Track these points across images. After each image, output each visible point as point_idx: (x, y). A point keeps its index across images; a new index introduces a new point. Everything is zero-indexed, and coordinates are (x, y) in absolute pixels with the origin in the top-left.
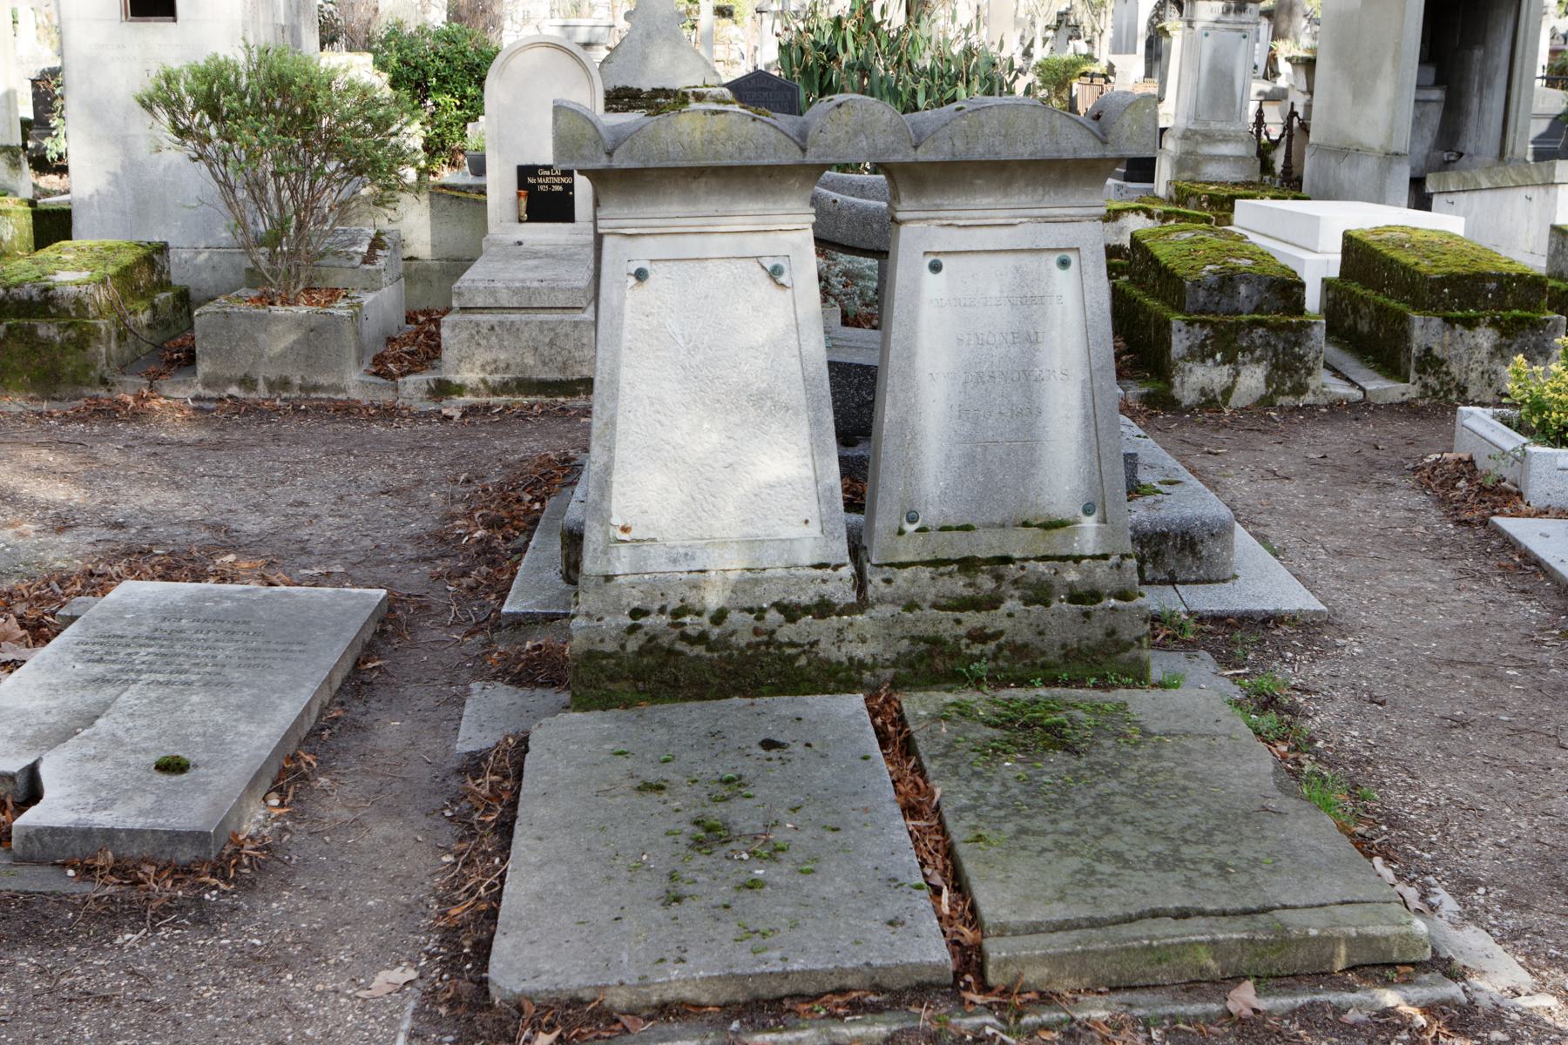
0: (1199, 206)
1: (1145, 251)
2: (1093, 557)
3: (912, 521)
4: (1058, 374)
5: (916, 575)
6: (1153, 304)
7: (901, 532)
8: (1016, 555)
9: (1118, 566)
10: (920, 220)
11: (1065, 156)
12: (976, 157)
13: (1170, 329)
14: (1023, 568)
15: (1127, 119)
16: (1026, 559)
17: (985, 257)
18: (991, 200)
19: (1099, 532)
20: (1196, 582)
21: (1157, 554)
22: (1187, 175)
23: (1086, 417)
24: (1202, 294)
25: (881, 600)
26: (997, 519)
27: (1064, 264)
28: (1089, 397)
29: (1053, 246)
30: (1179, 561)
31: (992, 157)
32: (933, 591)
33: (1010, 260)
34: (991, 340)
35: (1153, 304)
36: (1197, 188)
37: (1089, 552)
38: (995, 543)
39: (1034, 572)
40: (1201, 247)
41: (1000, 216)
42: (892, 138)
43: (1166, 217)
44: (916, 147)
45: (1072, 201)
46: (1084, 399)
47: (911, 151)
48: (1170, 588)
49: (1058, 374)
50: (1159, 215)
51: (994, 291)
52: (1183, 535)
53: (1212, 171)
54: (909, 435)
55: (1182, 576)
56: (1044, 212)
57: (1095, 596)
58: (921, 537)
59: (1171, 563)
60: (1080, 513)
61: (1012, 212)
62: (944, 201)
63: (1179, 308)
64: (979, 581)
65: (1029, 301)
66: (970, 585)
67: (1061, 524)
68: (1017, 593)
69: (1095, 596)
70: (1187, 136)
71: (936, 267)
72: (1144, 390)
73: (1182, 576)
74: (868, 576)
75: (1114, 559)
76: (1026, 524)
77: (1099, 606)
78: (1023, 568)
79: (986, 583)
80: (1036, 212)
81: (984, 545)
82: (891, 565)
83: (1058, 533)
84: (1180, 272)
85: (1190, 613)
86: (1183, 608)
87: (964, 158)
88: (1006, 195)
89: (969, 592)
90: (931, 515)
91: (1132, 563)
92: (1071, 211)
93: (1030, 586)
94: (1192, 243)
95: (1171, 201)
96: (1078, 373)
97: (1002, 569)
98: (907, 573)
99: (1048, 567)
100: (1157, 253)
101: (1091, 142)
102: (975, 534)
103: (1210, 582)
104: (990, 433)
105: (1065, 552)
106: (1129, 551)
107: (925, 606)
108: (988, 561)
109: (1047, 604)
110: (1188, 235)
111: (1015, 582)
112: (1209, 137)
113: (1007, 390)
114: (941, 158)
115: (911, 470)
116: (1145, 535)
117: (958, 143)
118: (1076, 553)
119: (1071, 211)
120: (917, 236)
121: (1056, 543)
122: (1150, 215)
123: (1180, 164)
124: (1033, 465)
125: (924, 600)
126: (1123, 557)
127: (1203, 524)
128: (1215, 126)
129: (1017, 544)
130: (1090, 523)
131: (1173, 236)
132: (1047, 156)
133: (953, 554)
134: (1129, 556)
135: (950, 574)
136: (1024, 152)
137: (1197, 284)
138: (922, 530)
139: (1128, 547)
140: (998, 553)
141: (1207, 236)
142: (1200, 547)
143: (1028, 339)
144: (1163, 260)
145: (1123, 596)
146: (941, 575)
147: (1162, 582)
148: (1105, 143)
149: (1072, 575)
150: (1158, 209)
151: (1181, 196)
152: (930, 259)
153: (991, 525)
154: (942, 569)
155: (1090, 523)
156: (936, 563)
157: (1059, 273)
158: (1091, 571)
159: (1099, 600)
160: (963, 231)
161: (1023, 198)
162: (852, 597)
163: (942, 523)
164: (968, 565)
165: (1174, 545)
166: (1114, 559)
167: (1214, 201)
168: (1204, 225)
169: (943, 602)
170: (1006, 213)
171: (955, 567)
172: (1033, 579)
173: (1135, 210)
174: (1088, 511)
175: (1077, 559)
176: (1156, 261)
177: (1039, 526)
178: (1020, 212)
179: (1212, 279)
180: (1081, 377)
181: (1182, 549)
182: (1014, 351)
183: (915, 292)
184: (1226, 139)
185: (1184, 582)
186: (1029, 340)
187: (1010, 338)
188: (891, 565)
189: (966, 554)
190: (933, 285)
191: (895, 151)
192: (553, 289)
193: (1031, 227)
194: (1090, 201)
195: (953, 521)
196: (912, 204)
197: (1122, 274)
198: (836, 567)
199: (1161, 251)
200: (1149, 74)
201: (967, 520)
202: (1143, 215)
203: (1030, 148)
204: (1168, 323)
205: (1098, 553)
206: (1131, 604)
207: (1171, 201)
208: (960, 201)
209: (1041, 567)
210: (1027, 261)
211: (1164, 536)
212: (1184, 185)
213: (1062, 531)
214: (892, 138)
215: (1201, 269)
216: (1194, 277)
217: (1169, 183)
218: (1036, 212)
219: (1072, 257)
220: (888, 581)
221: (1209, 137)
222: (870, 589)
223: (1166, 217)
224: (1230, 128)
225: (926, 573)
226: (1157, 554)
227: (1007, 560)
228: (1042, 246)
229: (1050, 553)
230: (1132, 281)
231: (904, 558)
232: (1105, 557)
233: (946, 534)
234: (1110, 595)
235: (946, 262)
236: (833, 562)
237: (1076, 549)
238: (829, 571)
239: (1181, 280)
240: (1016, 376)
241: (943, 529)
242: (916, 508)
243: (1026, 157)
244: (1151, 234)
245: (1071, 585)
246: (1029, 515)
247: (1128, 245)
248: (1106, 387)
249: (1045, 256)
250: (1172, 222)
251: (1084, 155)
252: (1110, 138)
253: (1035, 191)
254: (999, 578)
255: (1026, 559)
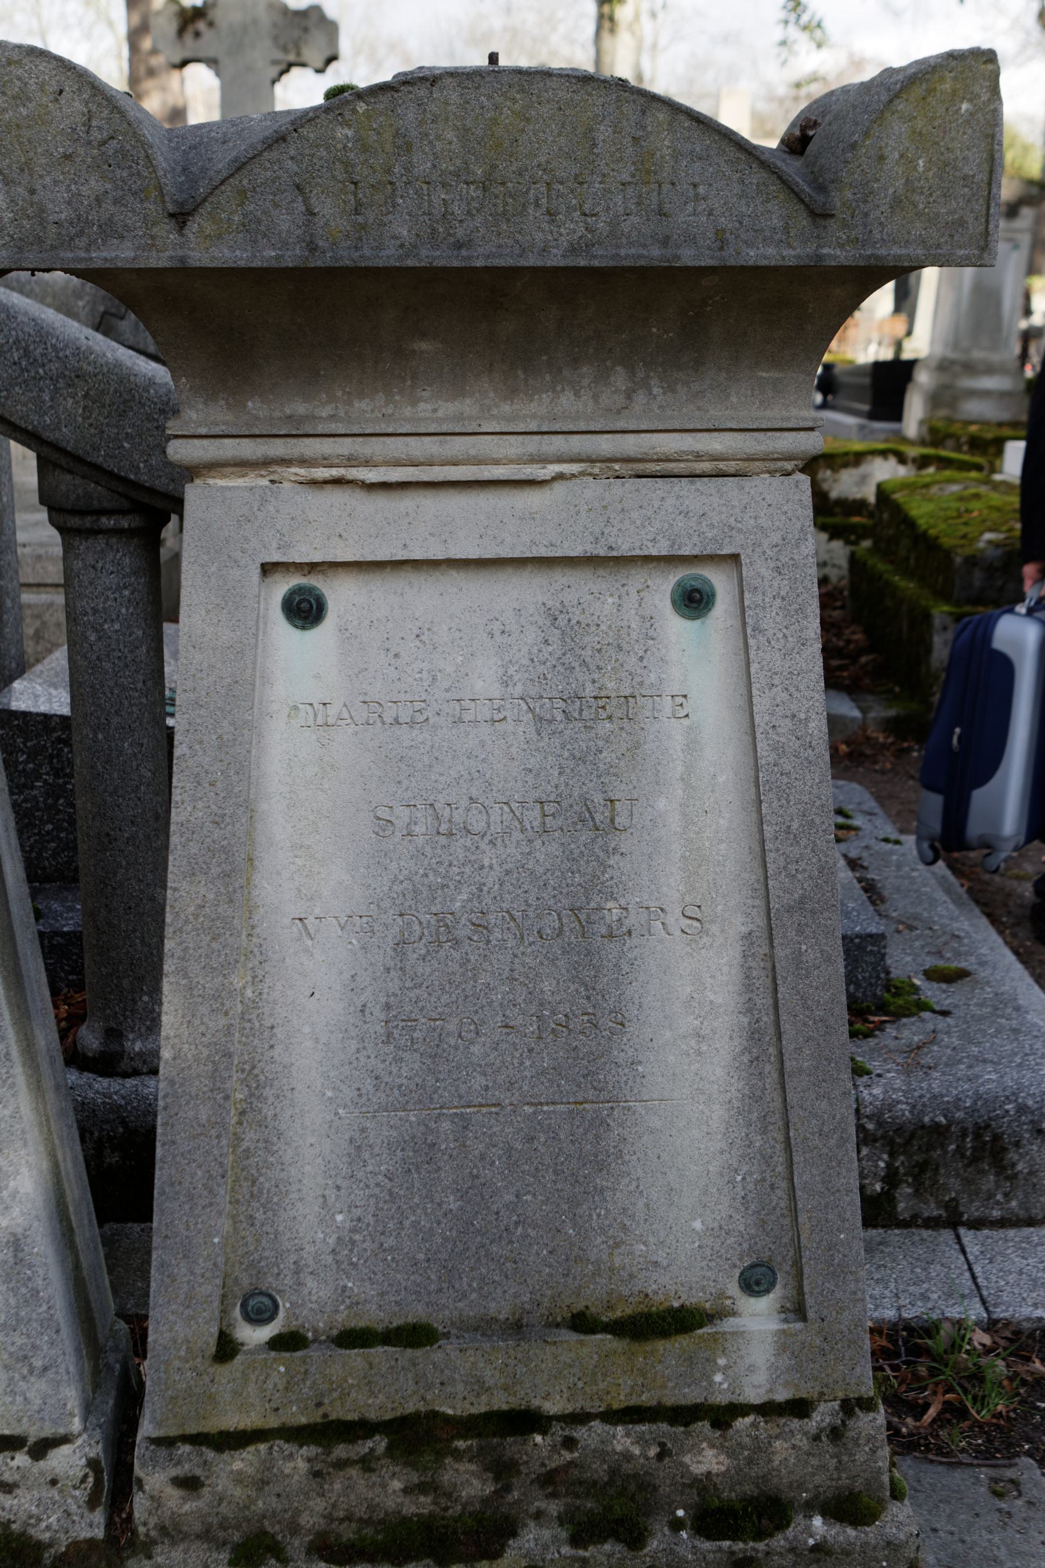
0: (958, 449)
1: (897, 509)
2: (768, 1410)
3: (258, 1317)
4: (674, 919)
5: (267, 1465)
6: (907, 586)
7: (226, 1348)
8: (551, 1407)
9: (836, 1434)
10: (243, 465)
11: (688, 257)
12: (388, 256)
13: (930, 625)
14: (570, 1443)
15: (896, 135)
16: (579, 1418)
17: (456, 577)
18: (467, 406)
19: (784, 1343)
20: (1002, 1223)
21: (922, 1167)
22: (943, 413)
23: (754, 1035)
24: (978, 577)
25: (171, 1532)
26: (501, 1308)
27: (694, 601)
28: (762, 982)
29: (662, 548)
30: (968, 1182)
31: (444, 258)
32: (319, 1505)
33: (528, 592)
34: (478, 824)
35: (907, 586)
36: (956, 428)
37: (753, 1396)
38: (491, 1376)
39: (602, 1454)
40: (975, 505)
41: (505, 457)
42: (95, 185)
43: (922, 462)
44: (180, 217)
45: (717, 414)
46: (748, 987)
47: (166, 232)
48: (947, 1235)
49: (674, 919)
50: (914, 460)
51: (484, 681)
52: (979, 1131)
53: (973, 408)
54: (247, 1086)
55: (973, 1210)
56: (630, 445)
57: (768, 1511)
58: (281, 1366)
59: (953, 1185)
60: (733, 1289)
61: (532, 445)
62: (324, 410)
63: (944, 595)
64: (446, 1477)
65: (588, 711)
66: (422, 1488)
67: (682, 1321)
68: (554, 1508)
69: (768, 1511)
70: (943, 366)
71: (304, 610)
72: (892, 713)
73: (973, 1210)
74: (138, 1471)
75: (823, 1415)
76: (582, 1323)
77: (779, 1541)
78: (570, 1443)
79: (468, 1482)
80: (605, 445)
81: (460, 1382)
82: (198, 1440)
83: (669, 1350)
84: (946, 542)
85: (991, 1326)
86: (975, 1312)
87: (347, 257)
88: (511, 393)
89: (423, 1505)
90: (314, 1299)
91: (873, 1423)
92: (716, 443)
93: (592, 1488)
94: (961, 499)
95: (922, 443)
96: (733, 919)
97: (511, 1447)
98: (242, 1461)
99: (641, 1440)
100: (914, 513)
101: (775, 213)
102: (436, 1355)
103: (1031, 1222)
104: (479, 1081)
105: (691, 1395)
106: (868, 1388)
107: (296, 1546)
108: (469, 1426)
109: (635, 1540)
110: (955, 488)
111: (549, 1480)
112: (970, 368)
113: (516, 971)
114: (267, 255)
115: (251, 1185)
116: (899, 1130)
117: (326, 208)
118: (721, 1399)
119: (716, 443)
120: (232, 522)
121: (664, 1372)
122: (902, 459)
123: (936, 399)
124: (601, 1167)
125: (294, 1529)
126: (849, 1407)
127: (1022, 1109)
128: (977, 355)
129: (556, 1377)
130: (758, 1317)
131: (934, 490)
132: (629, 254)
133: (376, 1406)
134: (867, 1405)
135: (366, 1464)
136: (548, 240)
137: (972, 561)
138: (288, 1342)
139: (863, 1380)
140: (501, 1402)
141: (983, 489)
142: (1012, 1155)
143: (586, 817)
144: (922, 523)
145: (850, 1508)
146: (341, 1464)
147: (933, 1223)
148: (820, 215)
149: (707, 1459)
150: (913, 452)
151: (935, 436)
152: (282, 586)
153: (484, 1327)
154: (341, 1451)
155: (758, 1317)
156: (326, 1432)
157: (677, 628)
158: (760, 1448)
159: (782, 1522)
160: (382, 501)
161: (567, 400)
162: (92, 1526)
163: (343, 1319)
164: (415, 1436)
165: (960, 1151)
166: (823, 1415)
167: (976, 444)
168: (974, 474)
169: (348, 1533)
170: (513, 446)
171: (379, 1443)
172: (599, 1470)
173: (884, 453)
174: (754, 1282)
175: (722, 1416)
176: (910, 523)
177: (618, 1328)
178: (558, 444)
179: (993, 553)
180: (739, 925)
181: (975, 1160)
182: (546, 854)
183: (242, 690)
184: (990, 370)
185: (977, 1224)
186: (587, 821)
187: (533, 817)
188: (198, 1440)
189: (410, 1408)
190: (300, 663)
191: (109, 230)
192: (39, 558)
193: (592, 490)
194: (774, 415)
195: (375, 1315)
196: (218, 414)
197: (863, 537)
198: (41, 1449)
199: (919, 510)
200: (898, 309)
201: (417, 1312)
202: (892, 461)
203: (572, 229)
204: (927, 617)
205: (781, 1396)
206: (871, 1533)
207: (922, 443)
208: (367, 409)
209: (622, 1439)
210: (576, 588)
211: (938, 1132)
212: (940, 424)
213: (681, 1343)
214: (95, 185)
215: (976, 539)
216: (968, 551)
217: (922, 423)
218: (605, 445)
219: (720, 580)
220: (190, 1484)
221: (970, 368)
222: (140, 1505)
223: (922, 462)
224: (996, 357)
225: (296, 1462)
226: (922, 1167)
227: (525, 1421)
228: (625, 548)
229: (646, 1399)
230: (875, 549)
231: (233, 1421)
232: (800, 1408)
233: (356, 1357)
234: (809, 1508)
235: (341, 595)
236: (34, 1432)
237: (720, 1387)
238: (21, 1459)
239: (948, 554)
240: (551, 922)
241: (353, 1338)
242: (269, 1282)
243: (556, 259)
244: (905, 486)
245: (703, 1485)
246: (592, 1296)
247: (872, 499)
248: (811, 956)
249: (637, 578)
250: (931, 470)
251: (753, 255)
252: (840, 199)
253: (602, 377)
254: (503, 1470)
255: (579, 1418)
